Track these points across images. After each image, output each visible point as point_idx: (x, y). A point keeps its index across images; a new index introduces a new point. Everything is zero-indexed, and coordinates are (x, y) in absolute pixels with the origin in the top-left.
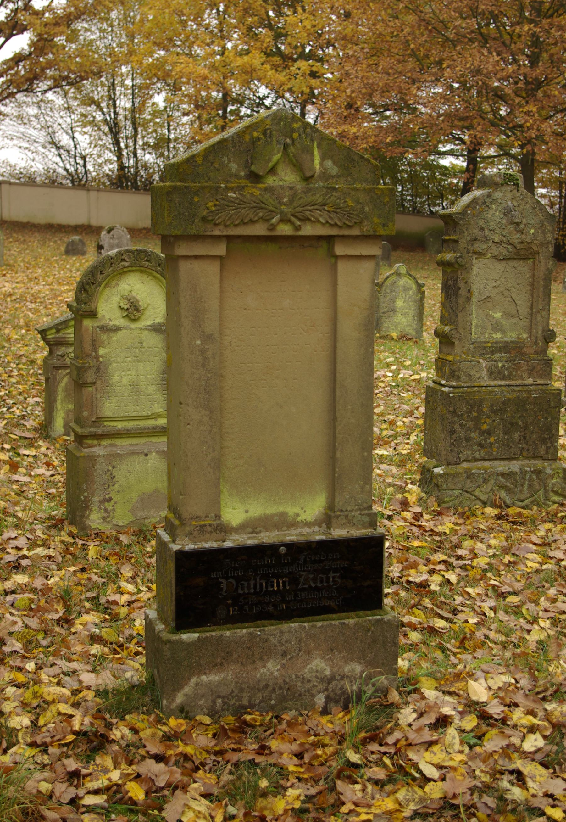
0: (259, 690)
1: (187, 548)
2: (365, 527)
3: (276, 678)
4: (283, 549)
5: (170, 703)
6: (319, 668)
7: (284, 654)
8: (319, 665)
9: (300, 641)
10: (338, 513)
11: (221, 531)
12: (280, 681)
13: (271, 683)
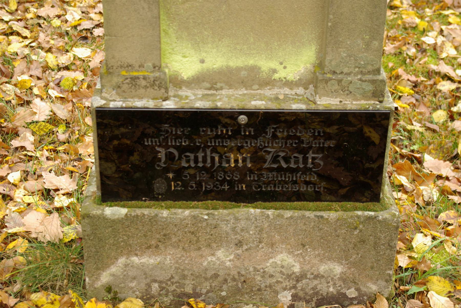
0: (206, 279)
1: (112, 105)
2: (365, 96)
3: (229, 269)
4: (243, 119)
5: (94, 281)
6: (285, 263)
7: (239, 244)
8: (285, 260)
9: (261, 231)
10: (329, 76)
11: (160, 87)
12: (234, 273)
13: (221, 273)
